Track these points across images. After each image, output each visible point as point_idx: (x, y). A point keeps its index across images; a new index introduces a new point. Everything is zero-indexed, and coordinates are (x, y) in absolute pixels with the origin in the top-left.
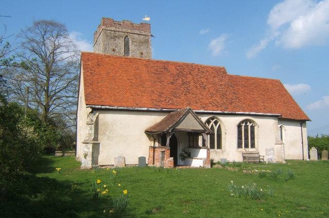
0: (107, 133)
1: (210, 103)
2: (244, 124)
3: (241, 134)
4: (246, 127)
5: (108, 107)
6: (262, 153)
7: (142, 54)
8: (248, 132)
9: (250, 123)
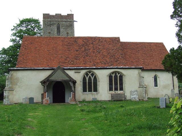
0: (18, 84)
2: (113, 75)
4: (116, 77)
5: (75, 68)
7: (68, 33)
8: (117, 80)
9: (119, 74)
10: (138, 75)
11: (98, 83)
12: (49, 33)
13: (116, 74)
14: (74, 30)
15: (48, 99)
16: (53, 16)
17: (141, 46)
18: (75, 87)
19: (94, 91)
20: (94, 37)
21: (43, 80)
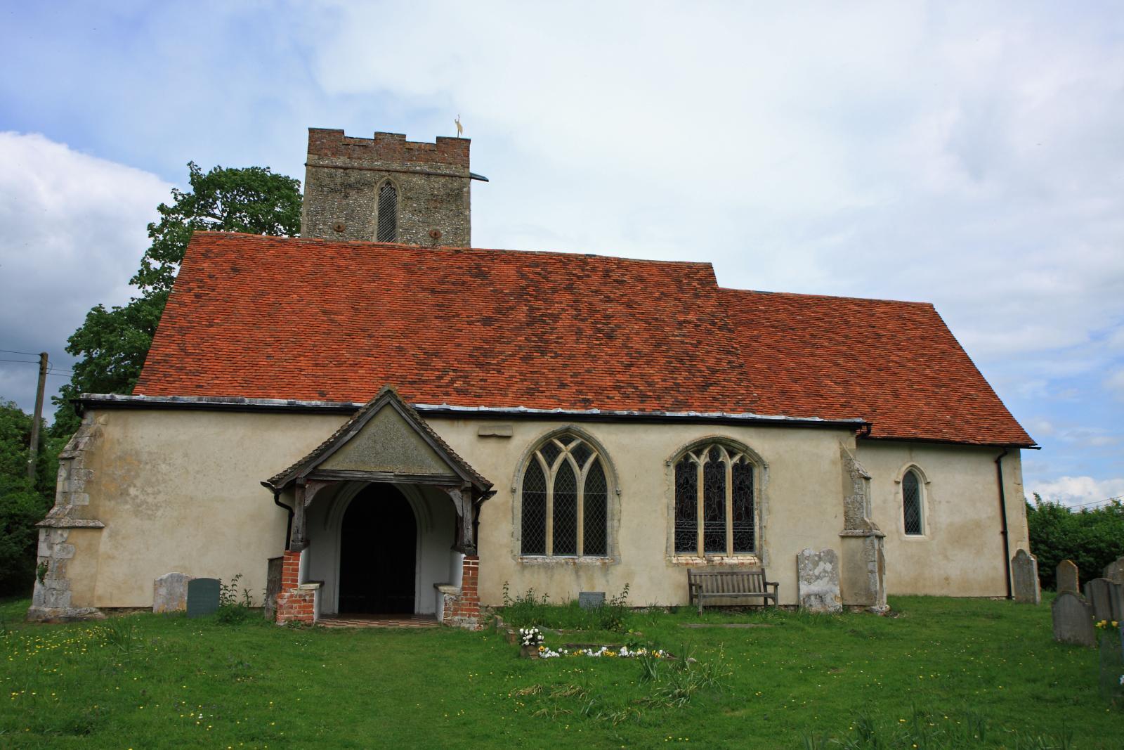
0: (132, 491)
1: (614, 388)
2: (702, 461)
3: (693, 498)
4: (715, 468)
6: (780, 572)
9: (732, 454)
10: (839, 468)
11: (612, 505)
12: (339, 229)
13: (714, 455)
14: (469, 222)
15: (309, 593)
16: (361, 144)
17: (825, 314)
18: (476, 524)
19: (588, 551)
20: (576, 256)
21: (285, 474)
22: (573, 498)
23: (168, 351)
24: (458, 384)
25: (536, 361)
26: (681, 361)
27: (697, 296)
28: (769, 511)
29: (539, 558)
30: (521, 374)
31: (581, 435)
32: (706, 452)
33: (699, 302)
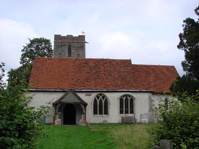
2: (124, 98)
3: (123, 105)
4: (127, 99)
7: (79, 55)
9: (130, 97)
11: (109, 106)
13: (126, 97)
16: (64, 37)
18: (85, 110)
22: (102, 105)
23: (32, 80)
24: (83, 85)
25: (97, 80)
26: (124, 79)
27: (128, 66)
28: (136, 107)
29: (97, 115)
30: (94, 82)
31: (103, 94)
32: (125, 97)
33: (128, 68)
